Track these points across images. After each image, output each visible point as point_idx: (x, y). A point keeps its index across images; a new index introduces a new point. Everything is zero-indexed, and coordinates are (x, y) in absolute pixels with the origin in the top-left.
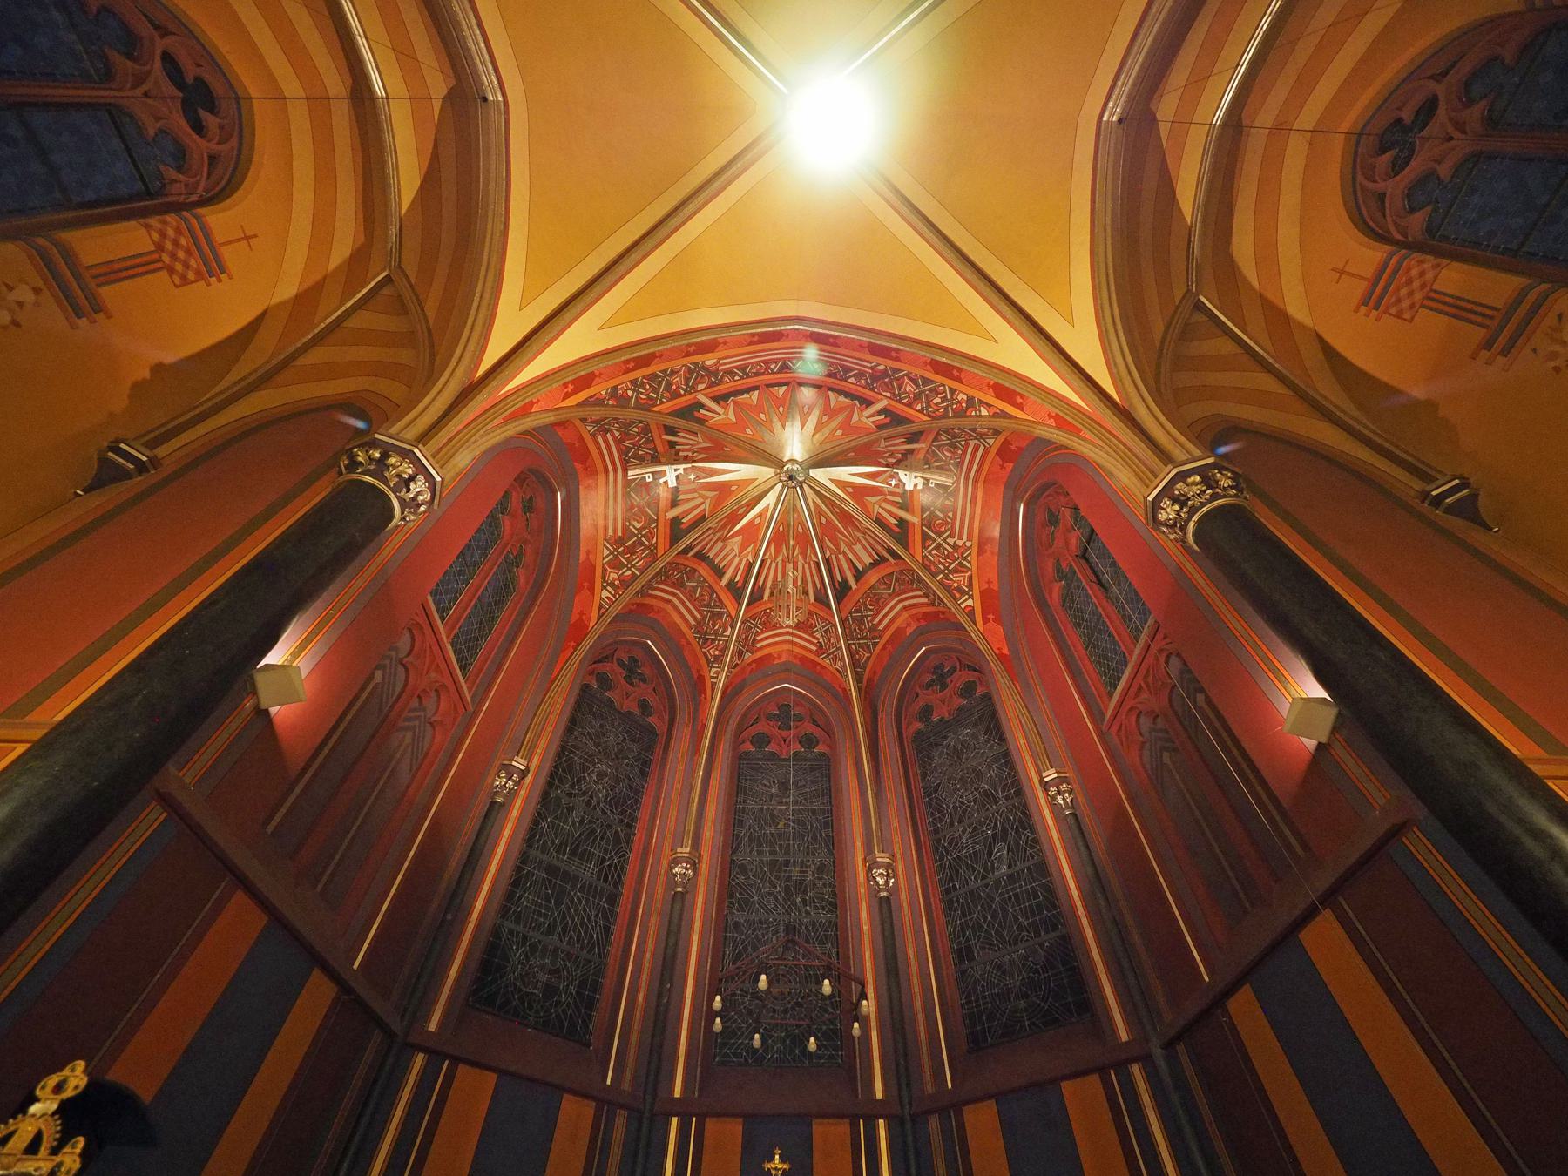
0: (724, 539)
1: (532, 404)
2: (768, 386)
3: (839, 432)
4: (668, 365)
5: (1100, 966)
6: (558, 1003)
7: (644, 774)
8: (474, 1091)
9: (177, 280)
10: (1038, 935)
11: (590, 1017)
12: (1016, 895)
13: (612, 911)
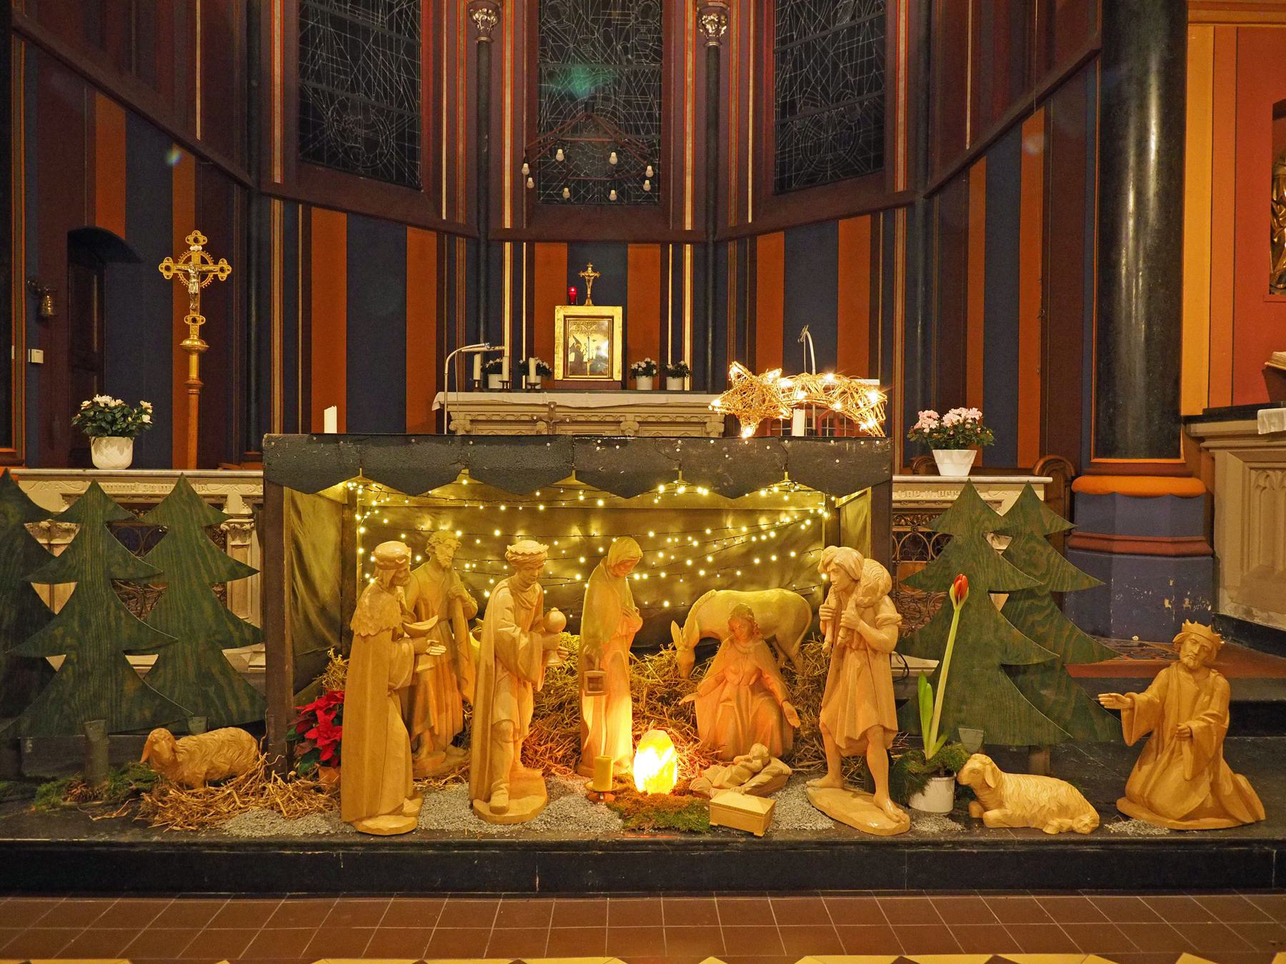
5: (901, 128)
6: (381, 154)
10: (860, 94)
11: (415, 165)
12: (851, 51)
13: (414, 64)
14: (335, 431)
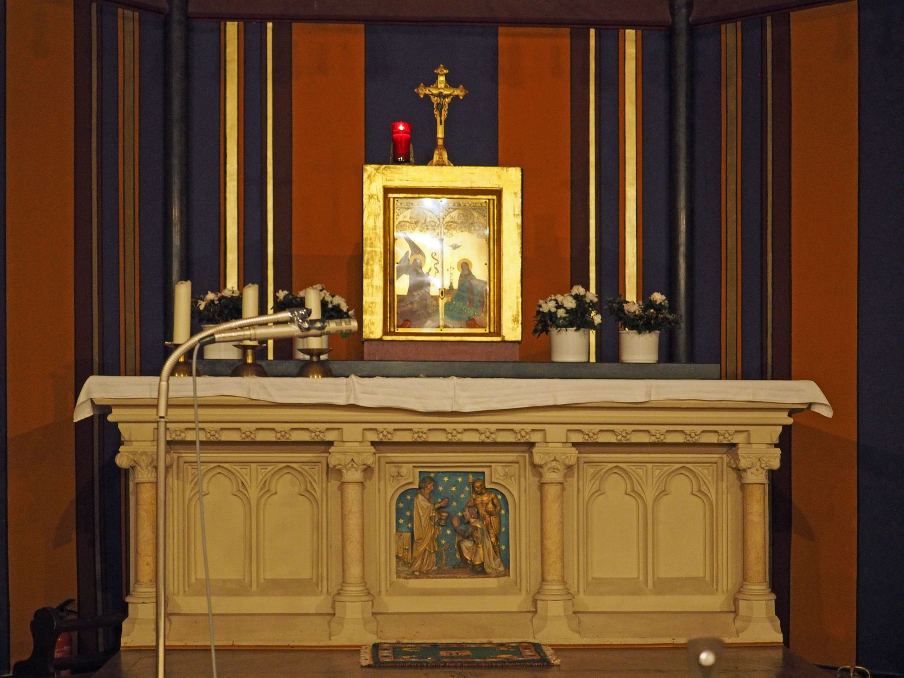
14: (627, 31)
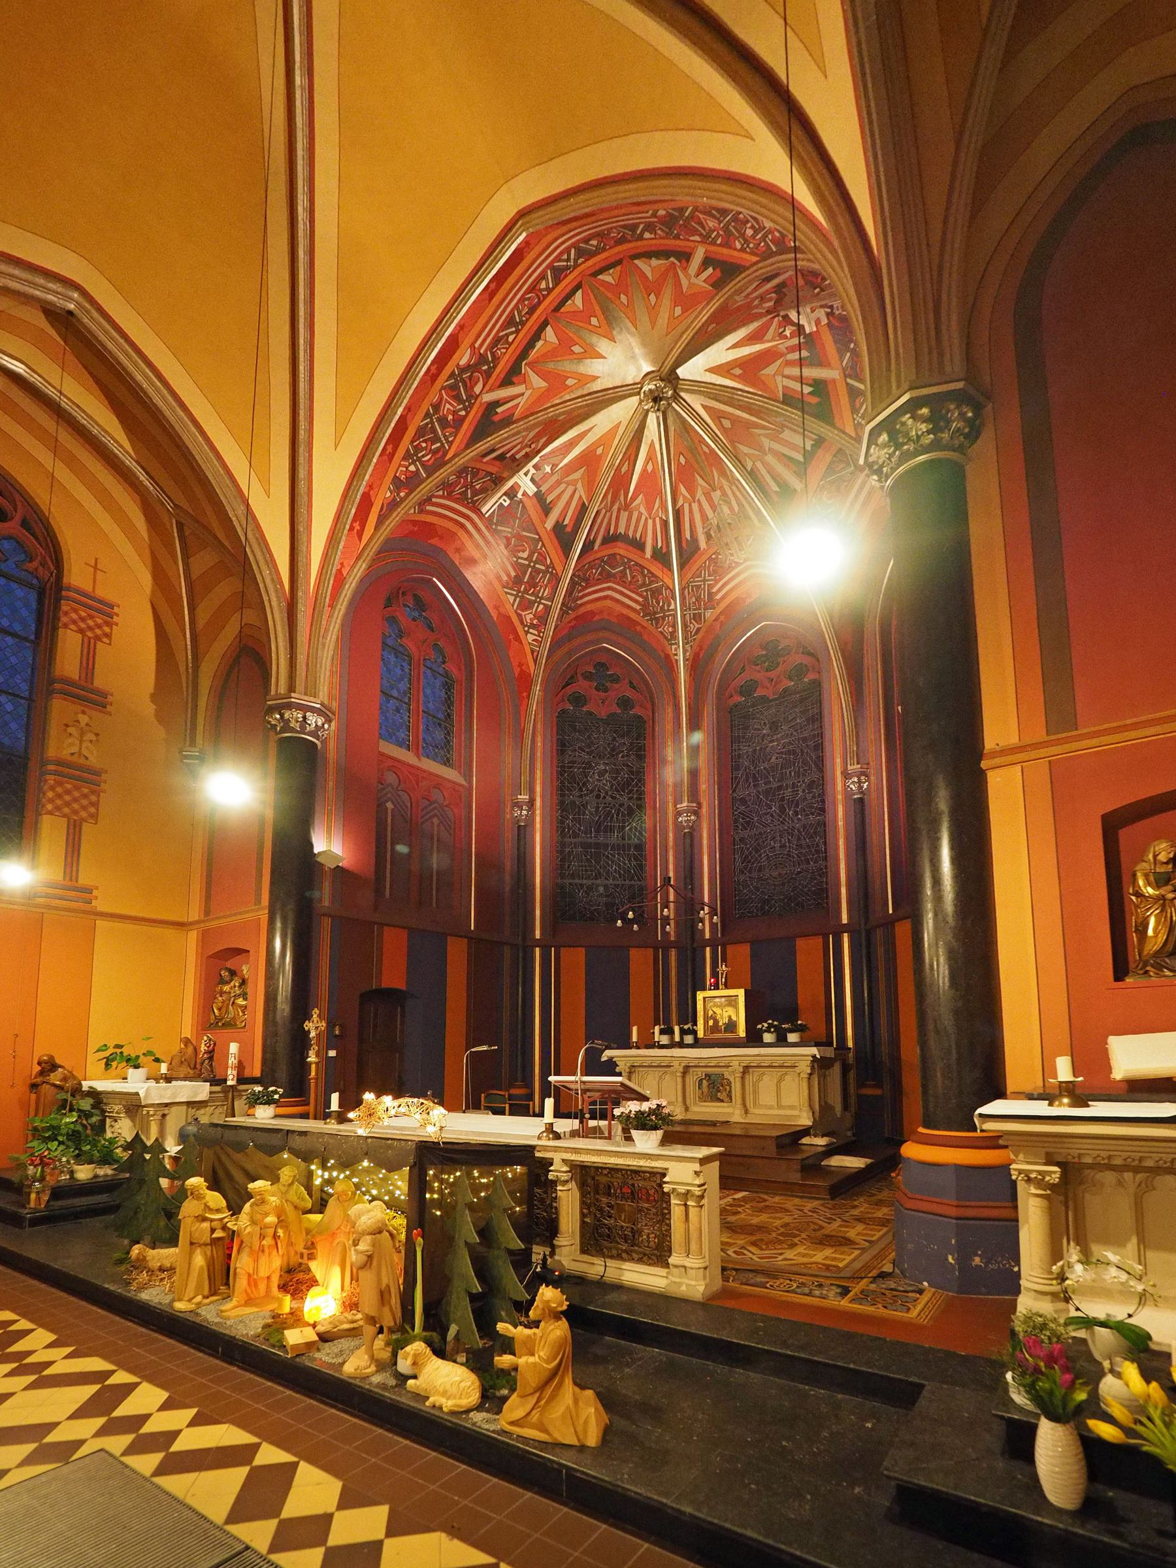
0: (627, 507)
1: (339, 571)
2: (557, 309)
3: (678, 311)
4: (426, 406)
7: (641, 758)
8: (575, 959)
9: (105, 640)
13: (641, 855)
